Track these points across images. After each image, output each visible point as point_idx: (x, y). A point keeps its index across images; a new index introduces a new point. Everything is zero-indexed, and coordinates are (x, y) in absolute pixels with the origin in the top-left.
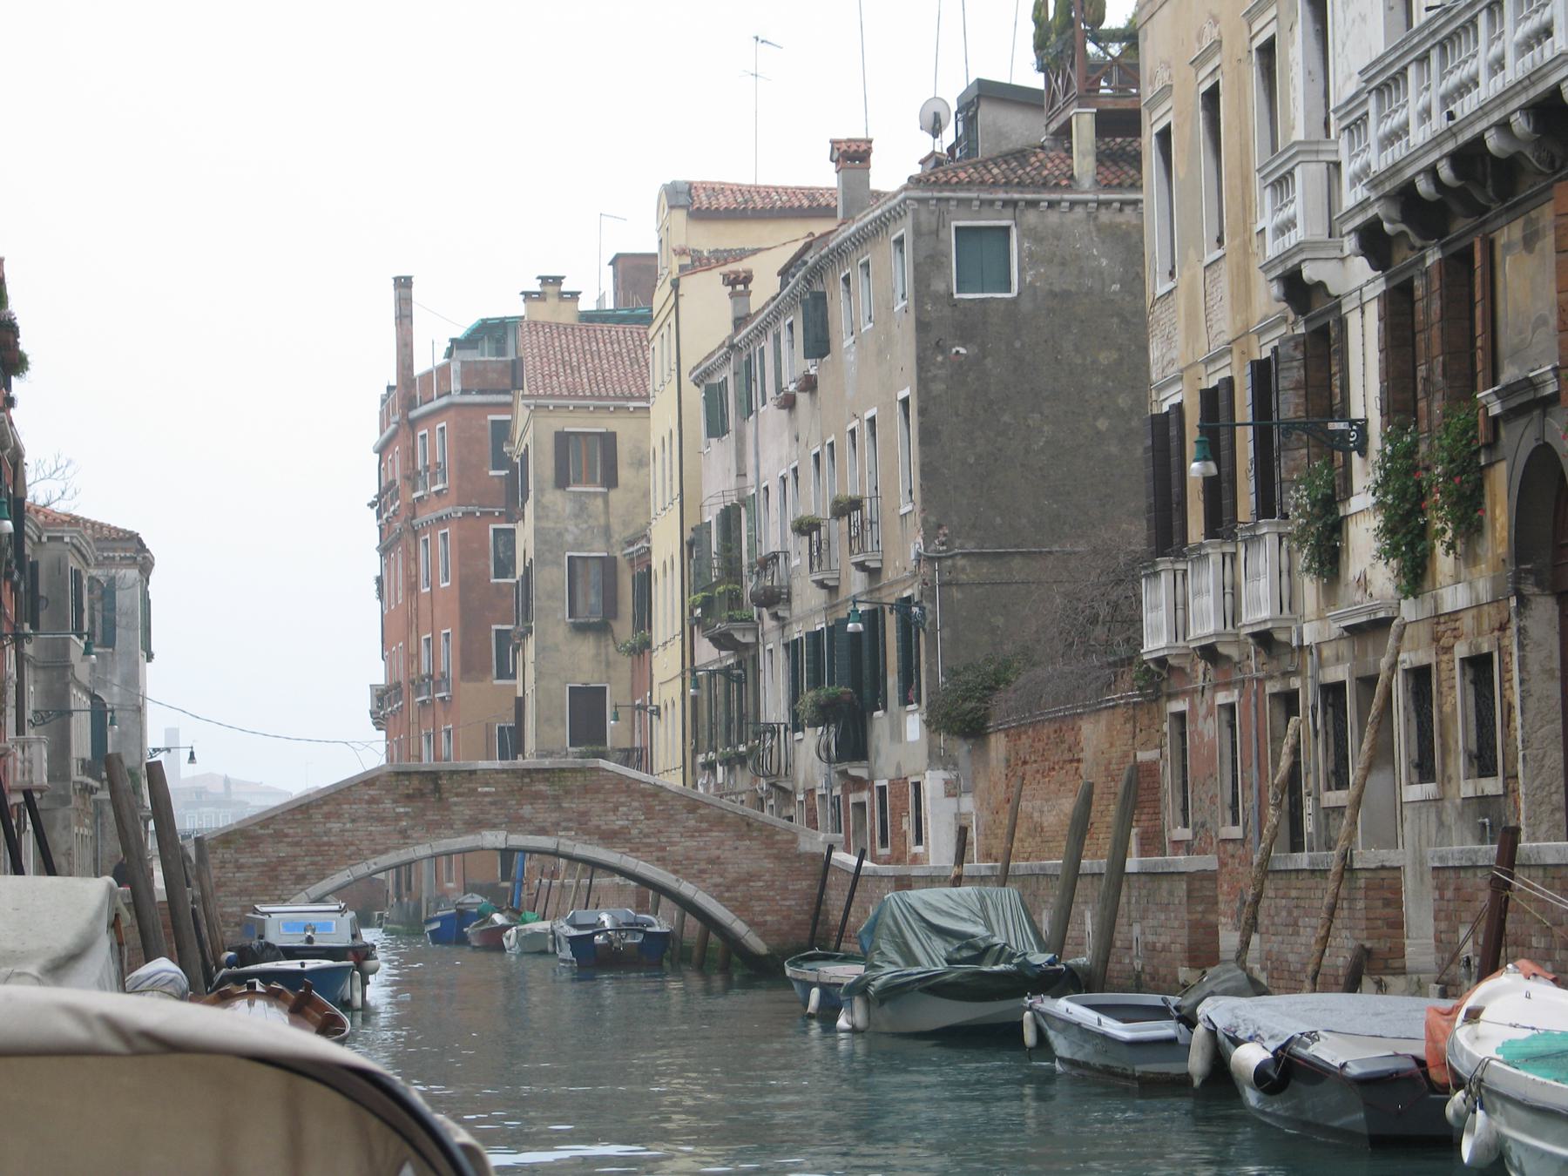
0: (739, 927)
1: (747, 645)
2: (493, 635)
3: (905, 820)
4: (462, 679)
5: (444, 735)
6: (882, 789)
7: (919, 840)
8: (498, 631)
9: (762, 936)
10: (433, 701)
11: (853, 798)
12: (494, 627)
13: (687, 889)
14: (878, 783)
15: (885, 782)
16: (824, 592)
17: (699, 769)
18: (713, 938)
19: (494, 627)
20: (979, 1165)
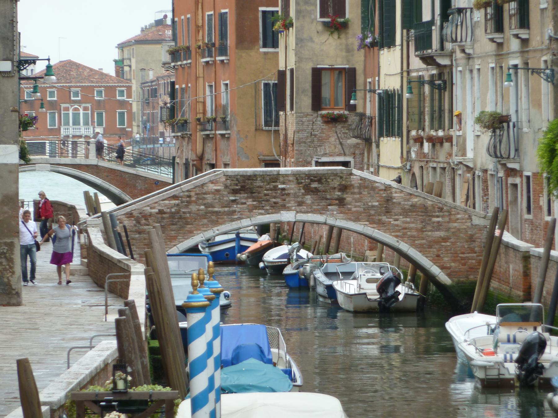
0: (435, 270)
1: (445, 66)
2: (260, 15)
3: (541, 199)
4: (237, 48)
5: (223, 88)
6: (528, 178)
7: (549, 213)
8: (264, 12)
9: (449, 275)
10: (215, 62)
11: (511, 180)
12: (261, 9)
13: (404, 247)
14: (526, 173)
15: (529, 174)
16: (494, 45)
17: (411, 142)
18: (419, 273)
19: (261, 9)
20: (277, 318)
